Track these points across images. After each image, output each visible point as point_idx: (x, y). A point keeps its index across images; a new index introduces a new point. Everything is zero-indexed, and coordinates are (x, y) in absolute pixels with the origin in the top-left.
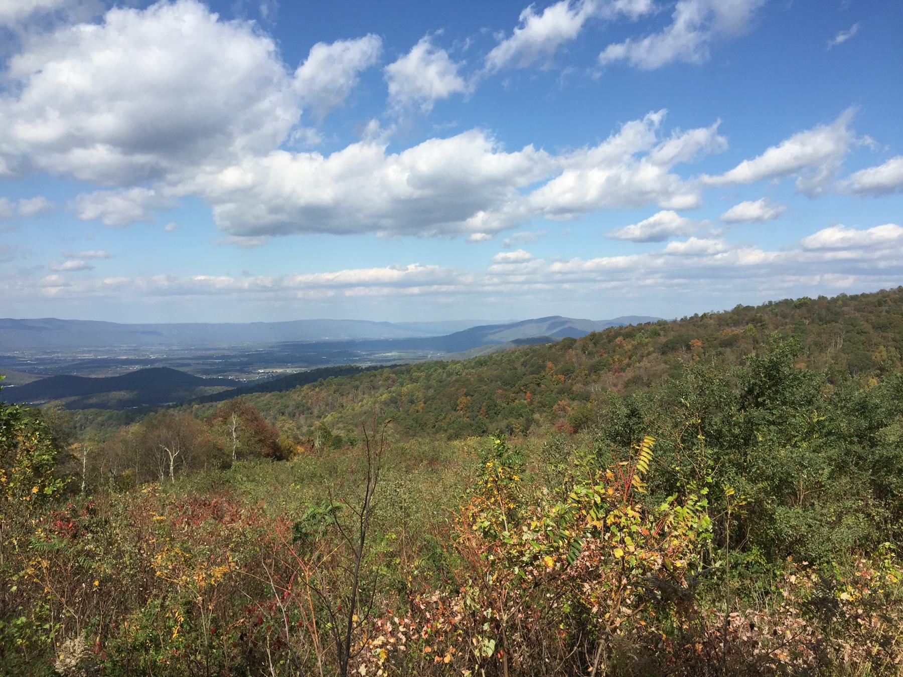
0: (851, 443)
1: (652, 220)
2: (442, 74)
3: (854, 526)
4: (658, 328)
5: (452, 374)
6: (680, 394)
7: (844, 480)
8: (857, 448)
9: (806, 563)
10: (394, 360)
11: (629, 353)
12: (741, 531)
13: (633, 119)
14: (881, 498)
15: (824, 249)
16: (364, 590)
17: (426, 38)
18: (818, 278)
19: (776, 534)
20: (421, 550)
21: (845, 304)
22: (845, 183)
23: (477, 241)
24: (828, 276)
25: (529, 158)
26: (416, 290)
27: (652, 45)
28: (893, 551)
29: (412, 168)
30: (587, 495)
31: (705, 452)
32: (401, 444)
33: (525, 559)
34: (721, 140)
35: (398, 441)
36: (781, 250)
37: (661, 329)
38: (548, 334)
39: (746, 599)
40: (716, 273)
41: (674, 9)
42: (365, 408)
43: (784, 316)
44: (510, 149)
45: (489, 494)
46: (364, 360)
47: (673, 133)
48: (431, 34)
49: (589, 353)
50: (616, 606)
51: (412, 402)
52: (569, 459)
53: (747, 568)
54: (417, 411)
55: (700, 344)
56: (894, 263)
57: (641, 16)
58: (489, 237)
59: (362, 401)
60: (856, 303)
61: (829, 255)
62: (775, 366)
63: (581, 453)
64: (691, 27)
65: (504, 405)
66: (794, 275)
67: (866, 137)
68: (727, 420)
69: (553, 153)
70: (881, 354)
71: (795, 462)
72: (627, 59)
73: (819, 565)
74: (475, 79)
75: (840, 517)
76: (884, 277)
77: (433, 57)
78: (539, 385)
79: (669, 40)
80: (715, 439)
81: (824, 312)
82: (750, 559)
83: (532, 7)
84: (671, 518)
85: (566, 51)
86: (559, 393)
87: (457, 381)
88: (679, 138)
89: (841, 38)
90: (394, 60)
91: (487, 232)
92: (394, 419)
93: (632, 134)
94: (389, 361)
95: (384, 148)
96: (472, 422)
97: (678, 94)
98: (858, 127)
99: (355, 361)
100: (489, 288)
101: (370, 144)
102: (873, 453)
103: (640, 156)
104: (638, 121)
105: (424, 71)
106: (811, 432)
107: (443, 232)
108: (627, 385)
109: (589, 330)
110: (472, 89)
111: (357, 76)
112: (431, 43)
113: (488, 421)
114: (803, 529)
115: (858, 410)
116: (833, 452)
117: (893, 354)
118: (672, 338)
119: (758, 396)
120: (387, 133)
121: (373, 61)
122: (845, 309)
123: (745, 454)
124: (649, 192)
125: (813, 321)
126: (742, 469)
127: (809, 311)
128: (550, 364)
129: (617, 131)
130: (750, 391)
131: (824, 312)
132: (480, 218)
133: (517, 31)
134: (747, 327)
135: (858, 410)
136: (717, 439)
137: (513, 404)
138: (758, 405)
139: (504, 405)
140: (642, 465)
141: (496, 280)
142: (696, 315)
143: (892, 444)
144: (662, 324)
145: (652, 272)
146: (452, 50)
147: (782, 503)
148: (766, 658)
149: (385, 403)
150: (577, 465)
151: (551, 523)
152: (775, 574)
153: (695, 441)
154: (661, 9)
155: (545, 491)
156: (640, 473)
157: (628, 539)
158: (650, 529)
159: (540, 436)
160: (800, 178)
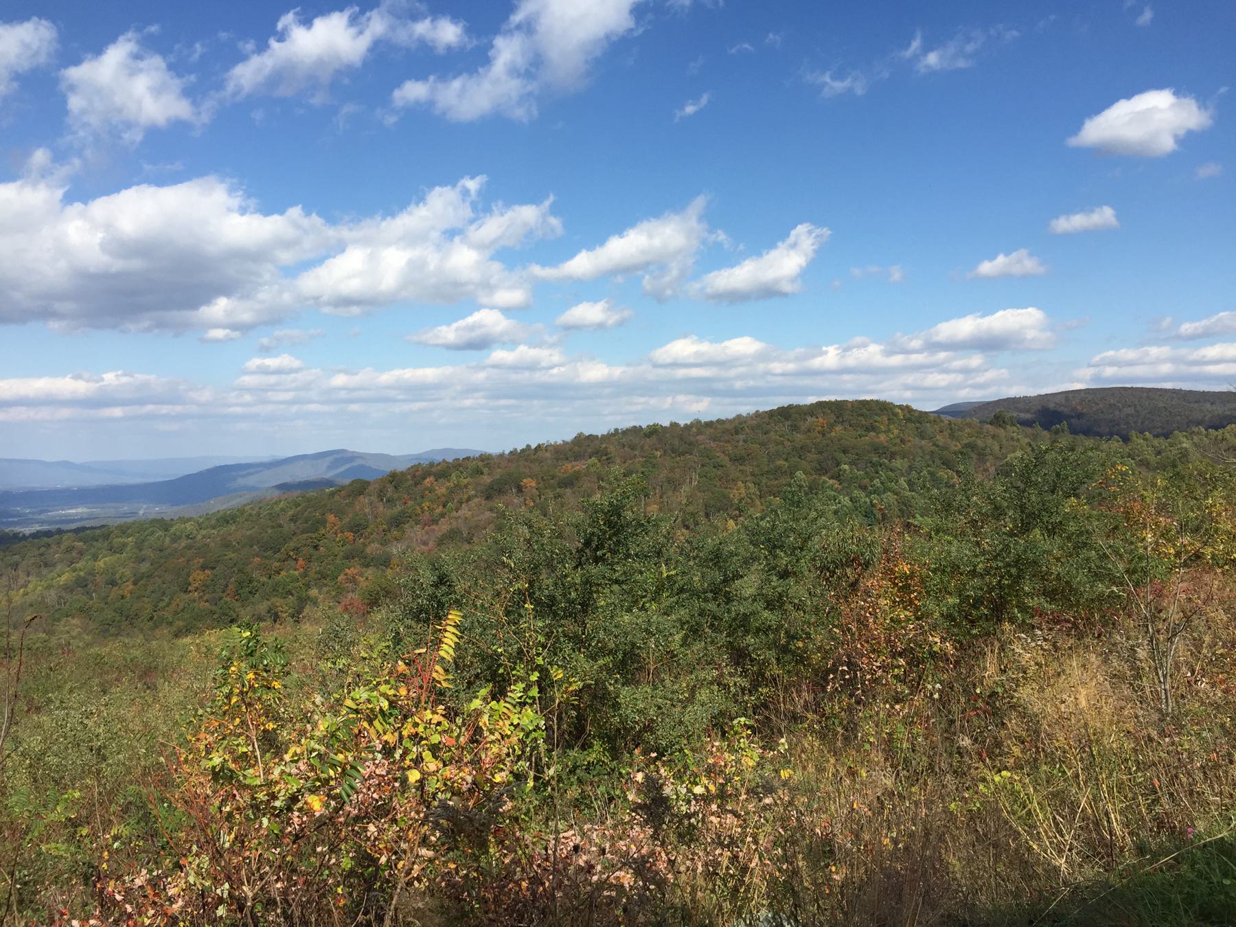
0: (706, 600)
1: (470, 320)
2: (157, 91)
3: (709, 700)
4: (480, 464)
5: (180, 538)
6: (503, 551)
7: (698, 646)
9: (654, 755)
10: (81, 519)
11: (443, 499)
12: (583, 725)
13: (443, 184)
14: (737, 664)
15: (675, 365)
16: (26, 884)
17: (130, 35)
18: (669, 400)
19: (621, 722)
20: (126, 810)
21: (699, 433)
22: (697, 286)
23: (217, 341)
24: (681, 398)
25: (297, 226)
26: (117, 412)
27: (464, 88)
28: (749, 727)
29: (108, 226)
30: (369, 701)
31: (533, 625)
32: (95, 650)
33: (278, 804)
34: (554, 221)
35: (88, 645)
36: (628, 365)
37: (485, 466)
38: (329, 475)
39: (586, 811)
40: (553, 392)
41: (491, 46)
42: (31, 598)
44: (266, 211)
45: (232, 713)
46: (27, 522)
48: (139, 30)
49: (388, 501)
50: (412, 850)
51: (113, 583)
52: (354, 650)
53: (588, 770)
54: (123, 597)
55: (533, 484)
56: (751, 383)
57: (449, 48)
58: (236, 334)
59: (25, 586)
61: (681, 373)
62: (616, 510)
63: (370, 642)
64: (513, 72)
65: (264, 579)
66: (642, 395)
67: (720, 232)
68: (561, 580)
69: (331, 220)
70: (738, 492)
72: (431, 103)
73: (671, 754)
74: (209, 104)
75: (693, 691)
77: (142, 64)
78: (316, 547)
79: (486, 85)
80: (546, 608)
81: (676, 442)
82: (592, 757)
83: (296, 14)
84: (486, 718)
85: (346, 81)
86: (347, 557)
87: (189, 547)
88: (502, 215)
89: (690, 109)
90: (77, 62)
91: (234, 327)
92: (83, 611)
93: (440, 205)
94: (73, 521)
95: (60, 193)
96: (214, 608)
97: (507, 157)
98: (711, 219)
99: (15, 524)
100: (238, 410)
101: (35, 185)
102: (729, 611)
103: (451, 234)
105: (124, 82)
106: (659, 590)
107: (161, 325)
108: (441, 542)
109: (388, 468)
110: (205, 118)
111: (13, 80)
112: (138, 42)
113: (238, 604)
114: (652, 712)
115: (712, 560)
116: (683, 613)
117: (752, 491)
119: (597, 549)
120: (63, 171)
121: (42, 59)
122: (700, 438)
123: (584, 624)
126: (579, 642)
127: (660, 440)
128: (331, 518)
129: (421, 199)
130: (587, 543)
131: (676, 442)
132: (221, 307)
133: (274, 44)
135: (712, 560)
136: (550, 607)
137: (278, 578)
138: (597, 560)
139: (264, 579)
140: (447, 651)
141: (248, 398)
142: (528, 446)
144: (485, 459)
145: (471, 390)
146: (172, 59)
148: (602, 885)
149: (68, 588)
150: (365, 659)
151: (317, 747)
152: (620, 773)
153: (522, 611)
154: (475, 42)
155: (318, 699)
157: (427, 755)
158: (458, 736)
159: (317, 622)
160: (647, 277)
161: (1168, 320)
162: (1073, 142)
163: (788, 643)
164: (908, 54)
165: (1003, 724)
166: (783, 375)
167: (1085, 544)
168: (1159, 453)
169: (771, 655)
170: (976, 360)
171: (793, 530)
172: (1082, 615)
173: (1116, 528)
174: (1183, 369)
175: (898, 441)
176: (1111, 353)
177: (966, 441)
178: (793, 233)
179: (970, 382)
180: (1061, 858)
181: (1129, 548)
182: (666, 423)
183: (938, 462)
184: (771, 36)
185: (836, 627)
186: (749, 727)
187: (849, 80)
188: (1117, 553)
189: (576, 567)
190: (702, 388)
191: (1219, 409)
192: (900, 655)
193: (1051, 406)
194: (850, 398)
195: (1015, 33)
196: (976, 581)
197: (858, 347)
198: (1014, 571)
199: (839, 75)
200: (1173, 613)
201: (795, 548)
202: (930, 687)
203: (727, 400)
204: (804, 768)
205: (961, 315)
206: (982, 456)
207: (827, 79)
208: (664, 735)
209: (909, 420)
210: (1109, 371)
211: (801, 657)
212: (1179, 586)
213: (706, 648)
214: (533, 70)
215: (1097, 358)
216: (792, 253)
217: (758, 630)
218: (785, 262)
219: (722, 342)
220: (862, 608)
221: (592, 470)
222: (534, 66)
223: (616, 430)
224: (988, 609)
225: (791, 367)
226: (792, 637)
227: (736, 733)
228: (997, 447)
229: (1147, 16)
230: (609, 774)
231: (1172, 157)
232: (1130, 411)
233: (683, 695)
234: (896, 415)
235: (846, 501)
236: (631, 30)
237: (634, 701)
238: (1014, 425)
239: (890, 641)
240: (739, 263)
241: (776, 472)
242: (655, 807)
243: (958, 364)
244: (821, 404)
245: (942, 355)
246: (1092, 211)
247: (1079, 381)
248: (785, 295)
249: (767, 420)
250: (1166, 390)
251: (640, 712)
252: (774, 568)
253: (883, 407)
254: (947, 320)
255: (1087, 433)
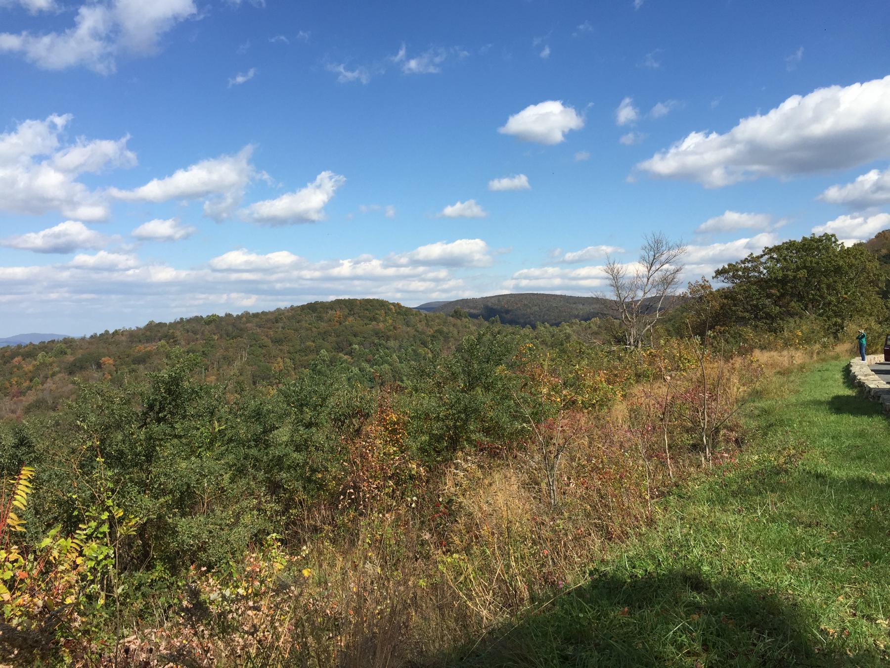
0: (249, 447)
1: (57, 229)
4: (64, 346)
8: (254, 452)
9: (204, 569)
11: (30, 375)
12: (146, 550)
13: (34, 117)
15: (230, 270)
18: (225, 296)
21: (248, 321)
22: (246, 212)
24: (234, 295)
28: (279, 540)
34: (130, 155)
36: (192, 269)
40: (128, 289)
43: (195, 333)
47: (78, 140)
55: (111, 361)
56: (288, 285)
57: (40, 11)
60: (258, 320)
61: (234, 276)
62: (175, 381)
64: (95, 35)
67: (264, 172)
68: (127, 438)
71: (195, 472)
75: (237, 516)
76: (280, 297)
79: (72, 43)
80: (116, 460)
81: (230, 328)
82: (155, 575)
88: (85, 146)
89: (240, 79)
93: (30, 134)
98: (257, 161)
102: (267, 454)
103: (39, 159)
104: (38, 121)
108: (28, 410)
114: (204, 536)
115: (254, 417)
118: (80, 356)
119: (160, 411)
122: (249, 325)
124: (52, 200)
125: (221, 337)
126: (144, 487)
127: (217, 327)
130: (151, 407)
131: (230, 328)
134: (159, 343)
135: (254, 417)
136: (119, 459)
138: (159, 420)
142: (107, 332)
143: (281, 444)
144: (69, 342)
145: (56, 285)
147: (183, 515)
153: (94, 464)
154: (63, 9)
156: (16, 509)
160: (207, 203)
161: (559, 250)
162: (502, 130)
163: (311, 475)
164: (397, 59)
165: (456, 521)
166: (311, 279)
167: (507, 397)
168: (553, 336)
169: (298, 485)
170: (443, 273)
171: (315, 392)
172: (500, 444)
173: (526, 384)
174: (566, 281)
175: (392, 328)
176: (525, 271)
177: (436, 328)
178: (319, 177)
179: (439, 288)
180: (486, 611)
181: (533, 398)
182: (222, 314)
183: (418, 343)
184: (301, 33)
185: (344, 461)
186: (279, 540)
187: (357, 71)
188: (525, 401)
189: (142, 426)
190: (250, 288)
191: (588, 309)
192: (390, 478)
193: (490, 305)
194: (359, 297)
195: (466, 53)
196: (440, 424)
197: (365, 261)
198: (463, 416)
199: (350, 68)
200: (559, 440)
201: (317, 406)
202: (409, 499)
203: (270, 298)
204: (321, 566)
205: (433, 241)
206: (446, 339)
207: (341, 69)
208: (213, 553)
209: (399, 313)
210: (524, 283)
211: (321, 485)
212: (562, 421)
213: (248, 484)
214: (112, 35)
215: (517, 274)
216: (318, 192)
217: (289, 467)
218: (313, 198)
219: (266, 254)
220: (364, 447)
221: (162, 350)
222: (113, 32)
223: (182, 319)
224: (444, 445)
225: (317, 274)
226: (314, 471)
227: (269, 545)
228: (455, 332)
229: (547, 52)
230: (168, 587)
231: (561, 146)
232: (536, 308)
233: (230, 520)
234: (390, 310)
235: (356, 370)
236: (193, 15)
237: (188, 528)
238: (466, 317)
239: (383, 469)
240: (279, 197)
241: (306, 351)
242: (198, 610)
243: (431, 275)
244: (338, 302)
245: (421, 269)
246: (514, 177)
247: (507, 289)
248: (313, 222)
249: (299, 312)
250: (557, 296)
251: (194, 537)
252: (302, 421)
253: (381, 305)
254: (424, 244)
255: (512, 322)
